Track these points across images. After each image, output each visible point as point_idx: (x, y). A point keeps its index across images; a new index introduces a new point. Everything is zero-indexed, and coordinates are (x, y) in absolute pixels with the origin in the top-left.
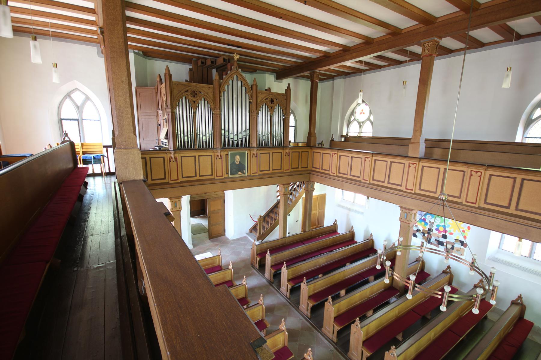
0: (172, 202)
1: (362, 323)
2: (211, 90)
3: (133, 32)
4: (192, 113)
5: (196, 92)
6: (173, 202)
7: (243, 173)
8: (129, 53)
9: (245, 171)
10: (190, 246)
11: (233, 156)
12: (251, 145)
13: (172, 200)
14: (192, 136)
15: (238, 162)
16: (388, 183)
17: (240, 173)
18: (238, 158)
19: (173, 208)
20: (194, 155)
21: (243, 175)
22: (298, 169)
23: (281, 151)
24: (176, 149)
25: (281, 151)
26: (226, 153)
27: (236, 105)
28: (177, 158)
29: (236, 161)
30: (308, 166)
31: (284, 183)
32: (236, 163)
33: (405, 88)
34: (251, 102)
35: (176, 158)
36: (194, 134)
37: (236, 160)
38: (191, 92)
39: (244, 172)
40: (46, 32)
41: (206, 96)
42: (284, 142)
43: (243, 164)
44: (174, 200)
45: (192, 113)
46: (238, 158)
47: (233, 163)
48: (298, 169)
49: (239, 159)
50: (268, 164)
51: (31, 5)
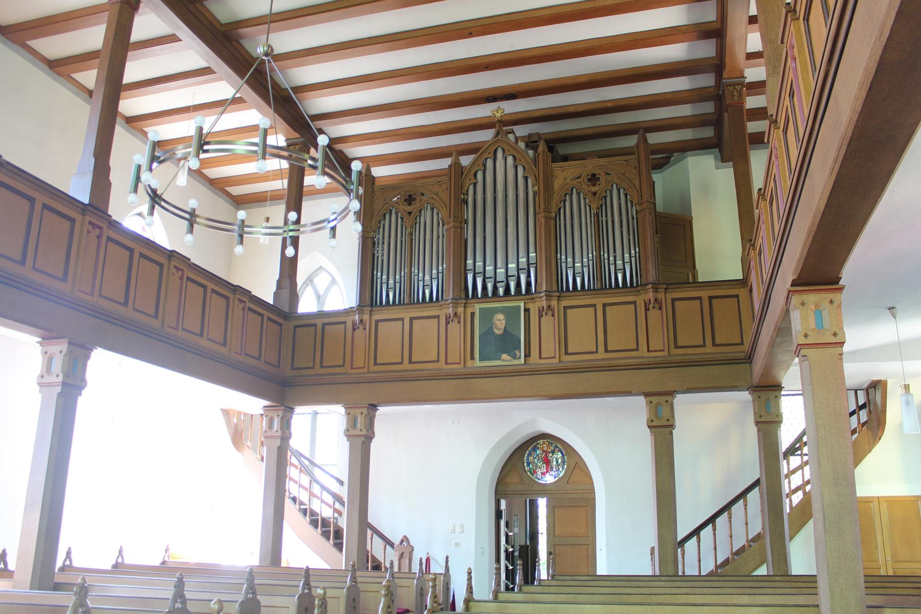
0: (651, 402)
5: (597, 185)
6: (363, 415)
7: (514, 357)
8: (116, 125)
9: (520, 352)
10: (56, 571)
11: (487, 315)
13: (349, 411)
15: (500, 329)
17: (504, 356)
18: (500, 321)
19: (349, 428)
20: (401, 316)
21: (515, 362)
22: (400, 367)
23: (630, 299)
25: (630, 299)
27: (579, 219)
28: (661, 300)
29: (496, 328)
30: (797, 346)
31: (647, 390)
33: (241, 243)
34: (536, 191)
36: (637, 254)
37: (495, 324)
38: (405, 198)
39: (518, 354)
41: (432, 198)
43: (515, 333)
44: (352, 411)
46: (500, 321)
47: (487, 333)
48: (400, 367)
49: (504, 322)
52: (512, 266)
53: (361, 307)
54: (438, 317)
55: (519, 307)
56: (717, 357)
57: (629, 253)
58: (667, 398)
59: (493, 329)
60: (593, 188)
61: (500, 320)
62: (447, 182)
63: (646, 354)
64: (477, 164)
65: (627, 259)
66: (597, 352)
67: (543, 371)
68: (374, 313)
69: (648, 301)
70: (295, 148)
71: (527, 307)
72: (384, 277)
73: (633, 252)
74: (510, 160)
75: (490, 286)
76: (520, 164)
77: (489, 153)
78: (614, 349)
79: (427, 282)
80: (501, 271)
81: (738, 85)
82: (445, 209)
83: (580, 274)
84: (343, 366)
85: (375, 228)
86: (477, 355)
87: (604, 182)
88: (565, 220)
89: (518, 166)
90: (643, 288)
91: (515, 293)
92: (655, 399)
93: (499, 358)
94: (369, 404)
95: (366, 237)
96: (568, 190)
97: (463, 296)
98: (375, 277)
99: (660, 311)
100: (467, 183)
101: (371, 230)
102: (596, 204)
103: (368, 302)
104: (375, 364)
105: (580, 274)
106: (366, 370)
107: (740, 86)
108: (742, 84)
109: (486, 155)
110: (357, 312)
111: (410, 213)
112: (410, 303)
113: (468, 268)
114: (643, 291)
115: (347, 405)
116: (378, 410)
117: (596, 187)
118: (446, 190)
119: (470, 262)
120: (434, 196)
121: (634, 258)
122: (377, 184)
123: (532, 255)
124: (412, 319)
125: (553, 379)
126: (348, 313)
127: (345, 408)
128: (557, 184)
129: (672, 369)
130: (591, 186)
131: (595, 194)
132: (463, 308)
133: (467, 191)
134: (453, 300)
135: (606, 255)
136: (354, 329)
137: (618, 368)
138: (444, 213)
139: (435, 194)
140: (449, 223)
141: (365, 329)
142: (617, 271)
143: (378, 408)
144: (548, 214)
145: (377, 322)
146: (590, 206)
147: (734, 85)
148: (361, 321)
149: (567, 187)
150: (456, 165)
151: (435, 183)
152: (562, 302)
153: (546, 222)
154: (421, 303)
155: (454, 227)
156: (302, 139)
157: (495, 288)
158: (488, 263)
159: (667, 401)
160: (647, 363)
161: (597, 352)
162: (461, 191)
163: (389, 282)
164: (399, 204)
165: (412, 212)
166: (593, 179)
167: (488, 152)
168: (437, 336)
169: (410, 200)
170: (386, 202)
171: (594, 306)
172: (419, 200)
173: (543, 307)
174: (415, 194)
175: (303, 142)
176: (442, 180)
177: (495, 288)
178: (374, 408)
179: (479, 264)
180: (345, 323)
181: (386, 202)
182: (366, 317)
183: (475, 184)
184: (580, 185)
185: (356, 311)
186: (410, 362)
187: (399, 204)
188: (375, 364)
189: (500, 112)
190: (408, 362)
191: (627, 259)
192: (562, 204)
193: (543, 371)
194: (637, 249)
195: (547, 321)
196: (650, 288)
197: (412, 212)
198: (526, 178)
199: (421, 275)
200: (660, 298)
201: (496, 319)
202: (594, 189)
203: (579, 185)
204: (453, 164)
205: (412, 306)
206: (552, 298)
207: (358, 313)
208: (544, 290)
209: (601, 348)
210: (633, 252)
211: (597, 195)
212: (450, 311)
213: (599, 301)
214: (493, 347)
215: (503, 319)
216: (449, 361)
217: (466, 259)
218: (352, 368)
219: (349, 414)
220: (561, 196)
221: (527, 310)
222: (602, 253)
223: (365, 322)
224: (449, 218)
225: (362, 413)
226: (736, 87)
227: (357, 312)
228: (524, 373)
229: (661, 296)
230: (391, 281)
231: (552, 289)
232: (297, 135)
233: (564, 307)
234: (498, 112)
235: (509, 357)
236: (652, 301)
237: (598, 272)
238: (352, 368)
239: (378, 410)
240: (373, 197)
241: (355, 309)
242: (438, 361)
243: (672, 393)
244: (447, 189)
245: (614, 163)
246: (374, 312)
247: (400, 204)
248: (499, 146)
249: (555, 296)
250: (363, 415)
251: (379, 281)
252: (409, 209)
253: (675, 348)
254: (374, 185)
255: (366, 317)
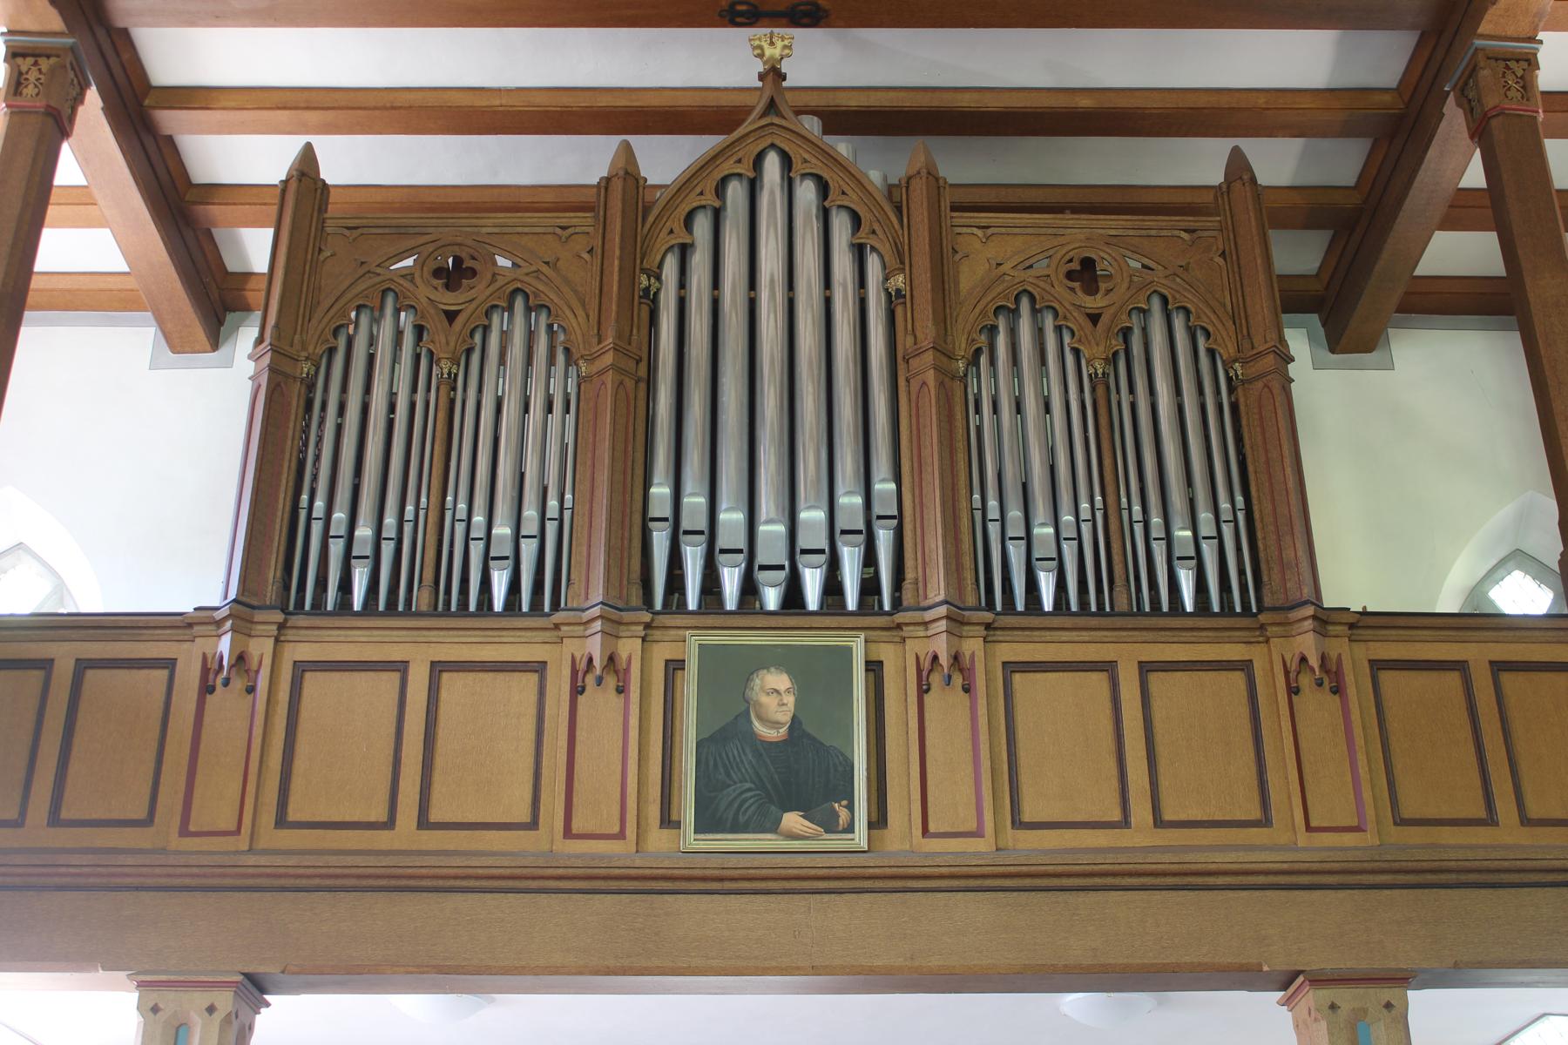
0: (1333, 1007)
1: (453, 325)
2: (580, 245)
3: (233, 104)
4: (429, 389)
6: (218, 1017)
7: (830, 824)
9: (851, 807)
12: (908, 597)
13: (154, 997)
14: (408, 528)
15: (776, 724)
16: (1522, 824)
20: (395, 654)
22: (382, 839)
24: (268, 603)
26: (662, 652)
29: (760, 718)
32: (752, 735)
34: (898, 291)
35: (958, 680)
37: (758, 704)
39: (843, 814)
40: (1291, 1000)
42: (1265, 578)
44: (170, 1000)
45: (429, 389)
49: (790, 700)
50: (1112, 764)
51: (51, 201)
52: (812, 516)
53: (244, 609)
54: (540, 668)
55: (847, 652)
56: (1167, 860)
57: (1073, 510)
58: (1387, 994)
59: (750, 722)
60: (1088, 299)
61: (777, 691)
62: (591, 229)
63: (176, 842)
64: (698, 190)
65: (530, 525)
66: (1125, 823)
67: (942, 877)
68: (290, 635)
69: (585, 661)
70: (36, 64)
71: (874, 658)
72: (339, 516)
73: (1084, 506)
74: (806, 193)
75: (731, 581)
76: (840, 207)
77: (739, 161)
78: (1183, 817)
79: (502, 548)
80: (772, 530)
81: (1518, 61)
82: (580, 313)
83: (822, 558)
84: (149, 821)
85: (319, 351)
86: (687, 812)
87: (1125, 285)
88: (344, 388)
89: (834, 212)
90: (1278, 617)
91: (861, 603)
92: (1346, 997)
93: (774, 827)
94: (246, 975)
95: (286, 375)
96: (1006, 298)
97: (636, 598)
98: (303, 514)
99: (1337, 697)
100: (663, 241)
101: (304, 354)
102: (1101, 348)
103: (271, 593)
104: (281, 822)
105: (822, 558)
106: (242, 843)
107: (1524, 65)
108: (1528, 60)
109: (728, 167)
110: (228, 624)
111: (451, 316)
112: (433, 613)
113: (655, 512)
114: (1275, 629)
115: (138, 973)
116: (268, 1005)
117: (1099, 296)
118: (586, 256)
119: (661, 490)
120: (545, 269)
121: (998, 524)
122: (332, 210)
123: (884, 487)
124: (438, 669)
125: (975, 910)
126: (190, 625)
127: (141, 985)
128: (969, 276)
129: (1396, 892)
130: (1080, 293)
131: (1094, 318)
132: (271, 641)
133: (660, 266)
134: (240, 607)
135: (1137, 508)
136: (207, 689)
137: (1211, 880)
138: (577, 324)
139: (547, 263)
140: (591, 359)
141: (251, 690)
142: (492, 563)
143: (267, 997)
144: (945, 359)
145: (301, 669)
146: (1077, 353)
147: (1505, 60)
148: (240, 659)
149: (1001, 288)
150: (627, 174)
151: (550, 230)
152: (998, 646)
153: (941, 385)
154: (472, 615)
155: (613, 366)
156: (70, 41)
157: (749, 589)
158: (724, 502)
159: (1388, 1006)
160: (1315, 866)
161: (1125, 823)
162: (642, 262)
163: (357, 533)
164: (412, 281)
165: (457, 313)
166: (1086, 273)
167: (735, 158)
168: (532, 736)
169: (454, 276)
170: (365, 268)
171: (401, 667)
172: (489, 276)
173: (590, 660)
174: (474, 258)
175: (72, 49)
176: (574, 221)
177: (749, 589)
178: (256, 993)
179: (695, 500)
180: (170, 664)
181: (365, 268)
182: (261, 648)
183: (685, 251)
184: (1048, 288)
185: (225, 619)
186: (424, 823)
187: (412, 281)
188: (281, 822)
189: (779, 44)
190: (415, 824)
191: (530, 525)
192: (478, 338)
193: (942, 877)
194: (1098, 498)
195: (600, 704)
196: (1305, 619)
197: (457, 313)
198: (859, 252)
199: (479, 519)
200: (1333, 655)
201: (762, 688)
202: (1093, 303)
203: (1042, 284)
204: (621, 173)
205: (443, 623)
206: (967, 628)
207: (233, 629)
208: (941, 597)
209: (1141, 811)
210: (1084, 506)
211: (1104, 320)
212: (595, 647)
213: (1127, 655)
214: (748, 785)
215: (788, 691)
216: (576, 827)
217: (647, 484)
218: (184, 831)
219: (155, 1009)
220: (983, 313)
221: (874, 667)
222: (1124, 500)
223: (254, 666)
224: (595, 340)
225: (211, 1009)
226: (1512, 64)
227: (228, 624)
228: (472, 883)
229: (973, 646)
230: (364, 532)
231: (964, 602)
232: (55, 21)
233: (1004, 663)
234: (772, 43)
235: (807, 823)
236: (597, 663)
237: (1117, 558)
238: (184, 831)
239: (268, 1005)
240: (320, 250)
241: (218, 615)
242: (533, 824)
243: (1403, 979)
244: (590, 251)
245: (1153, 232)
246: (290, 632)
247: (418, 280)
248: (773, 146)
249: (978, 624)
250: (218, 1017)
251: (317, 528)
252: (450, 300)
253: (1395, 824)
254: (326, 211)
255: (261, 648)
